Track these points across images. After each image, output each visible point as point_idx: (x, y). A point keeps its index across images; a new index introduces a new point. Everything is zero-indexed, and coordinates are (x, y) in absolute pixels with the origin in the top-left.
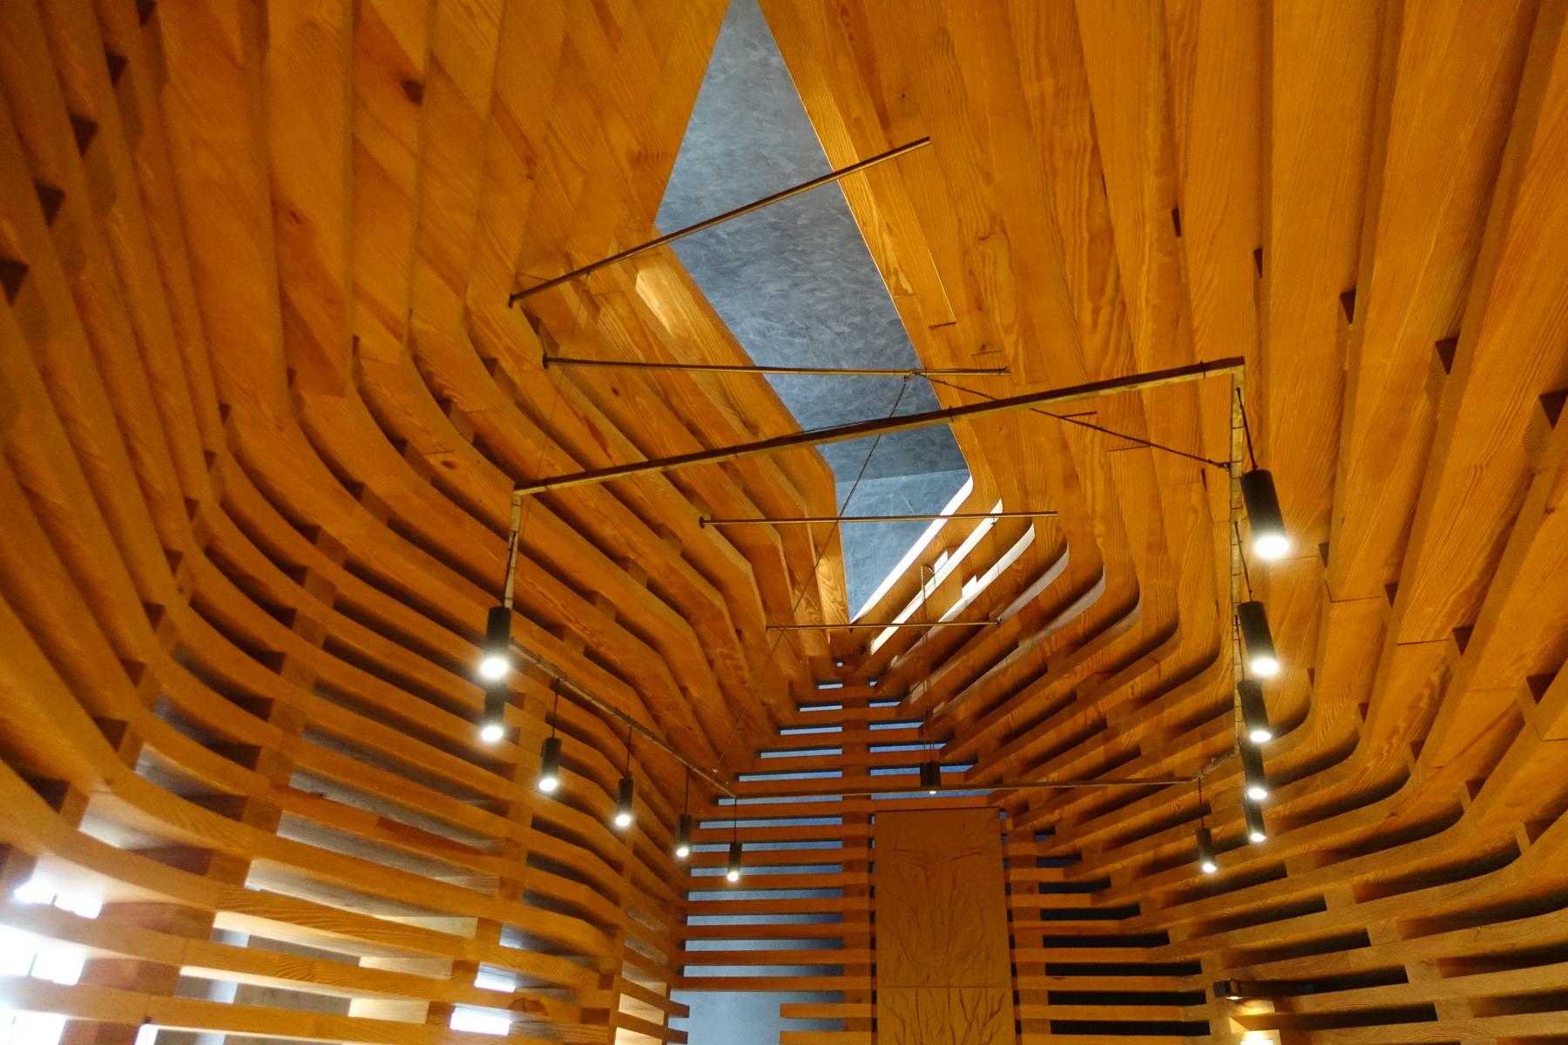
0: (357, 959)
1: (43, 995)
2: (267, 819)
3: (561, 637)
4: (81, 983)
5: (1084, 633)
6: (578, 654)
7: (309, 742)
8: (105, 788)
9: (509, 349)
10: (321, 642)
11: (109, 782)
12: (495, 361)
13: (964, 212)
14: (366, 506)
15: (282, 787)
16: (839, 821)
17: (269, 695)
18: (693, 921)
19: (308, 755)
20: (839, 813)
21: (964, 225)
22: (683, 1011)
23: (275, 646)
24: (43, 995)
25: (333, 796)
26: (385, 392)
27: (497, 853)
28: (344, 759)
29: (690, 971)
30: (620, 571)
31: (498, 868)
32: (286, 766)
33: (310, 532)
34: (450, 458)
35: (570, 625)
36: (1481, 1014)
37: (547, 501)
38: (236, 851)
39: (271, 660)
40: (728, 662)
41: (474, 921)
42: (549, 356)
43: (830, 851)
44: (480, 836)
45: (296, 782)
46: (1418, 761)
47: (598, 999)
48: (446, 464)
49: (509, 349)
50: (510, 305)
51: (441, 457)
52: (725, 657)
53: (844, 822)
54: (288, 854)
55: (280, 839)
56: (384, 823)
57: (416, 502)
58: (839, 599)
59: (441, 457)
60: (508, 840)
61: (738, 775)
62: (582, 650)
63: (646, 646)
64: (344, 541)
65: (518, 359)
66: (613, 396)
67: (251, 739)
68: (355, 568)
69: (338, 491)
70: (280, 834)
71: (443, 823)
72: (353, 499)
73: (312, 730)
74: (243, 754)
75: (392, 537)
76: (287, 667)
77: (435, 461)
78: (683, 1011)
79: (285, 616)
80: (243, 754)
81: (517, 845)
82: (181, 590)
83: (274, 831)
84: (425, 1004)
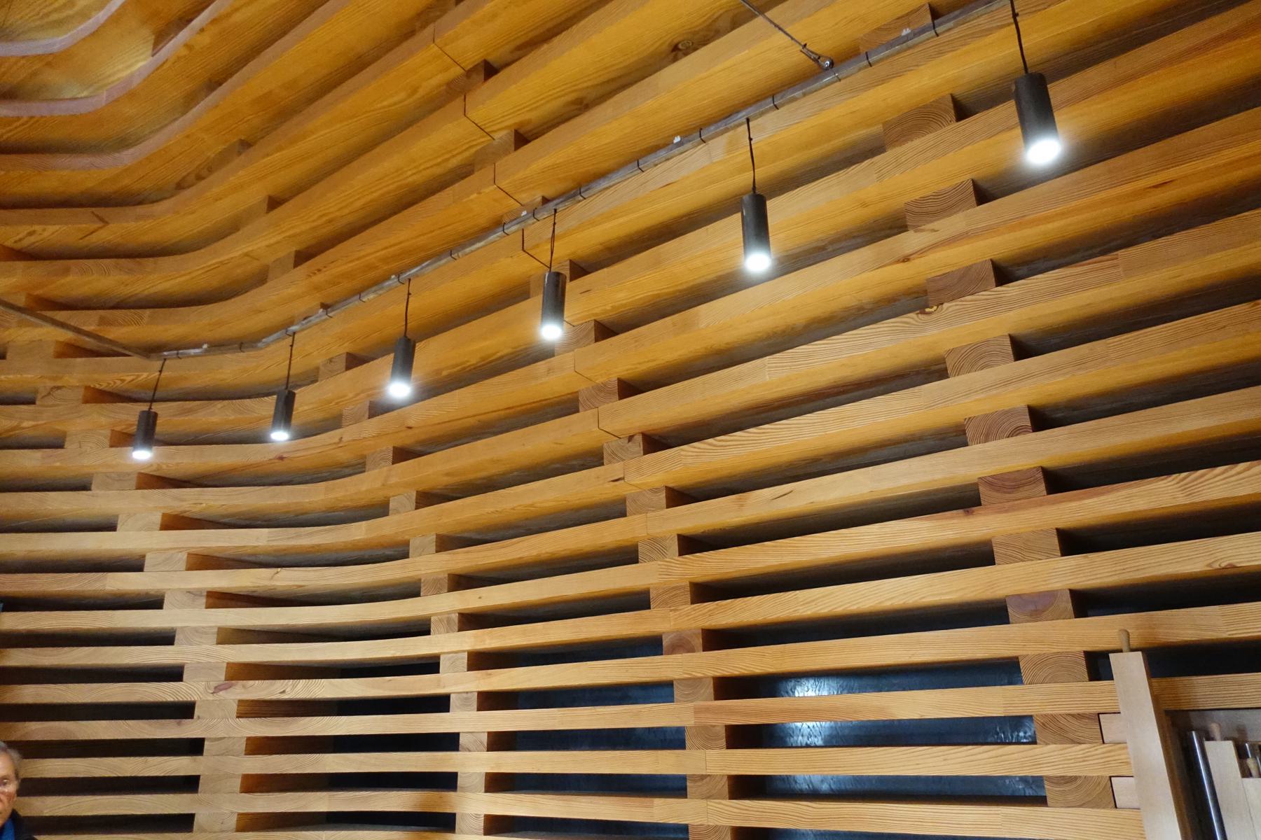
36: (222, 641)
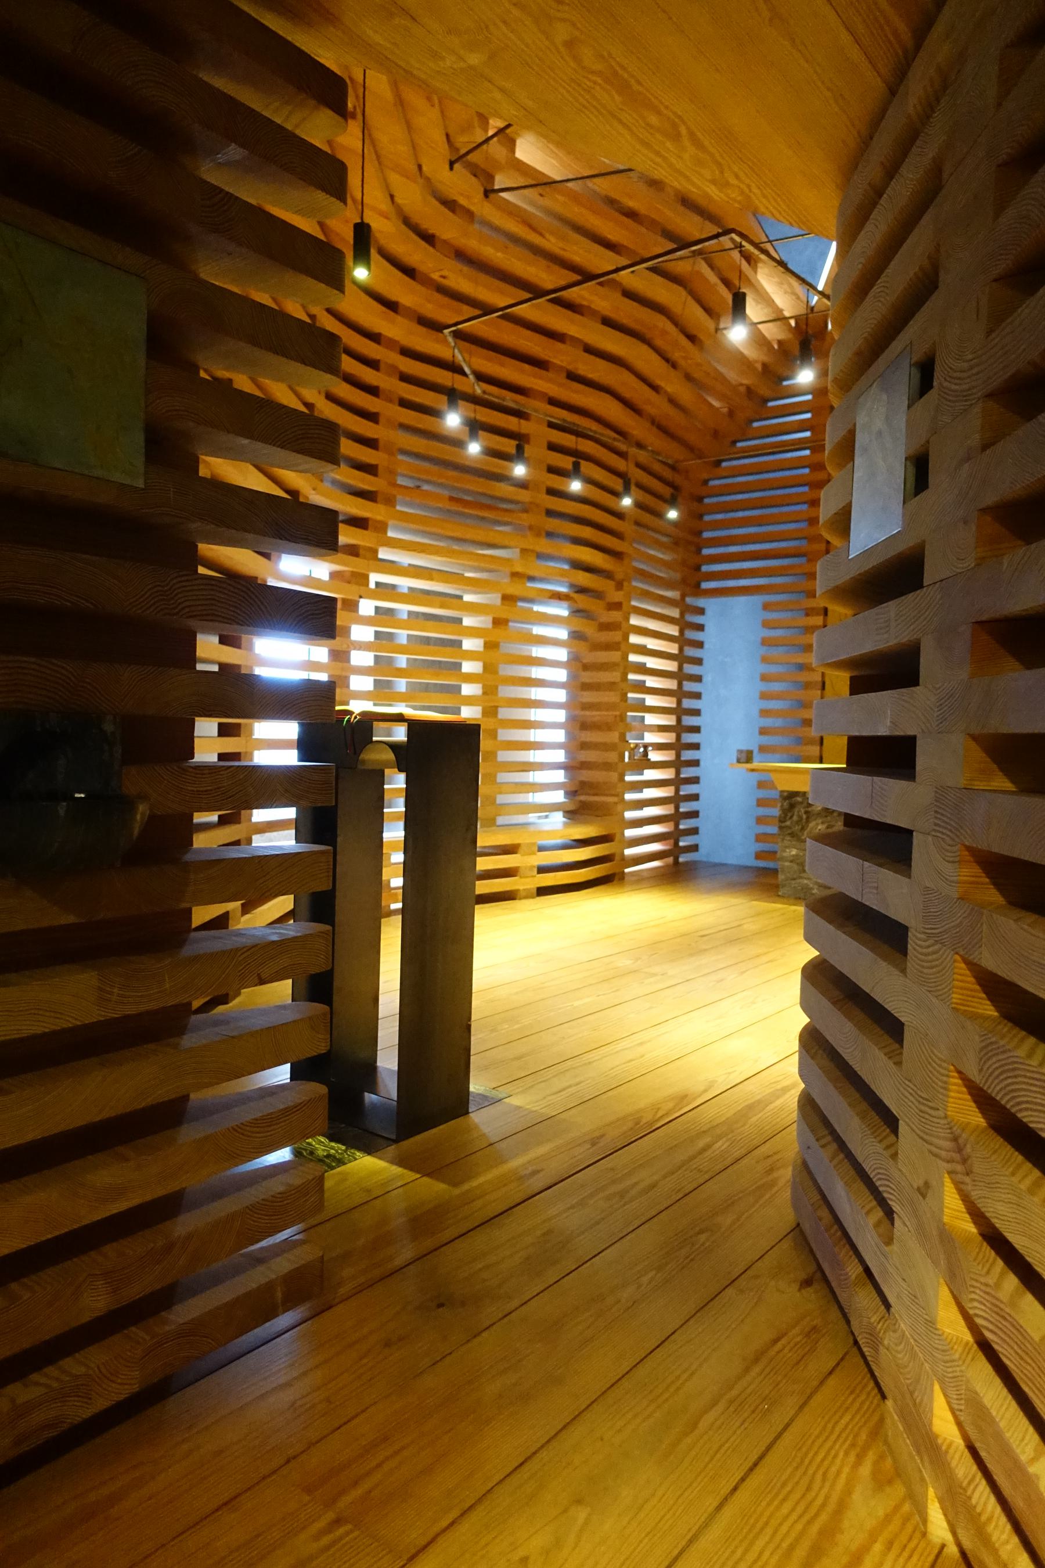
0: (644, 682)
2: (390, 501)
3: (547, 370)
8: (314, 492)
11: (314, 489)
14: (403, 316)
15: (394, 485)
16: (807, 471)
17: (375, 436)
18: (706, 552)
20: (807, 464)
21: (630, 125)
22: (701, 611)
23: (373, 410)
25: (425, 487)
26: (394, 246)
27: (525, 511)
28: (426, 465)
29: (705, 585)
30: (577, 317)
31: (526, 519)
32: (392, 473)
33: (375, 337)
34: (445, 273)
35: (551, 360)
38: (379, 518)
39: (372, 417)
40: (689, 361)
41: (518, 550)
42: (489, 188)
43: (798, 494)
44: (511, 502)
45: (400, 481)
46: (922, 400)
47: (617, 596)
48: (444, 277)
50: (451, 168)
51: (438, 274)
52: (685, 358)
53: (811, 471)
54: (404, 517)
55: (398, 511)
56: (452, 499)
57: (430, 306)
58: (789, 290)
59: (438, 274)
60: (531, 503)
61: (734, 442)
62: (564, 375)
63: (614, 366)
64: (397, 338)
65: (468, 197)
66: (541, 198)
67: (373, 462)
68: (407, 352)
70: (398, 508)
71: (493, 497)
72: (392, 313)
74: (370, 469)
75: (423, 330)
76: (382, 420)
77: (435, 276)
78: (701, 611)
79: (373, 391)
80: (370, 469)
81: (537, 506)
82: (320, 393)
83: (394, 507)
84: (500, 596)
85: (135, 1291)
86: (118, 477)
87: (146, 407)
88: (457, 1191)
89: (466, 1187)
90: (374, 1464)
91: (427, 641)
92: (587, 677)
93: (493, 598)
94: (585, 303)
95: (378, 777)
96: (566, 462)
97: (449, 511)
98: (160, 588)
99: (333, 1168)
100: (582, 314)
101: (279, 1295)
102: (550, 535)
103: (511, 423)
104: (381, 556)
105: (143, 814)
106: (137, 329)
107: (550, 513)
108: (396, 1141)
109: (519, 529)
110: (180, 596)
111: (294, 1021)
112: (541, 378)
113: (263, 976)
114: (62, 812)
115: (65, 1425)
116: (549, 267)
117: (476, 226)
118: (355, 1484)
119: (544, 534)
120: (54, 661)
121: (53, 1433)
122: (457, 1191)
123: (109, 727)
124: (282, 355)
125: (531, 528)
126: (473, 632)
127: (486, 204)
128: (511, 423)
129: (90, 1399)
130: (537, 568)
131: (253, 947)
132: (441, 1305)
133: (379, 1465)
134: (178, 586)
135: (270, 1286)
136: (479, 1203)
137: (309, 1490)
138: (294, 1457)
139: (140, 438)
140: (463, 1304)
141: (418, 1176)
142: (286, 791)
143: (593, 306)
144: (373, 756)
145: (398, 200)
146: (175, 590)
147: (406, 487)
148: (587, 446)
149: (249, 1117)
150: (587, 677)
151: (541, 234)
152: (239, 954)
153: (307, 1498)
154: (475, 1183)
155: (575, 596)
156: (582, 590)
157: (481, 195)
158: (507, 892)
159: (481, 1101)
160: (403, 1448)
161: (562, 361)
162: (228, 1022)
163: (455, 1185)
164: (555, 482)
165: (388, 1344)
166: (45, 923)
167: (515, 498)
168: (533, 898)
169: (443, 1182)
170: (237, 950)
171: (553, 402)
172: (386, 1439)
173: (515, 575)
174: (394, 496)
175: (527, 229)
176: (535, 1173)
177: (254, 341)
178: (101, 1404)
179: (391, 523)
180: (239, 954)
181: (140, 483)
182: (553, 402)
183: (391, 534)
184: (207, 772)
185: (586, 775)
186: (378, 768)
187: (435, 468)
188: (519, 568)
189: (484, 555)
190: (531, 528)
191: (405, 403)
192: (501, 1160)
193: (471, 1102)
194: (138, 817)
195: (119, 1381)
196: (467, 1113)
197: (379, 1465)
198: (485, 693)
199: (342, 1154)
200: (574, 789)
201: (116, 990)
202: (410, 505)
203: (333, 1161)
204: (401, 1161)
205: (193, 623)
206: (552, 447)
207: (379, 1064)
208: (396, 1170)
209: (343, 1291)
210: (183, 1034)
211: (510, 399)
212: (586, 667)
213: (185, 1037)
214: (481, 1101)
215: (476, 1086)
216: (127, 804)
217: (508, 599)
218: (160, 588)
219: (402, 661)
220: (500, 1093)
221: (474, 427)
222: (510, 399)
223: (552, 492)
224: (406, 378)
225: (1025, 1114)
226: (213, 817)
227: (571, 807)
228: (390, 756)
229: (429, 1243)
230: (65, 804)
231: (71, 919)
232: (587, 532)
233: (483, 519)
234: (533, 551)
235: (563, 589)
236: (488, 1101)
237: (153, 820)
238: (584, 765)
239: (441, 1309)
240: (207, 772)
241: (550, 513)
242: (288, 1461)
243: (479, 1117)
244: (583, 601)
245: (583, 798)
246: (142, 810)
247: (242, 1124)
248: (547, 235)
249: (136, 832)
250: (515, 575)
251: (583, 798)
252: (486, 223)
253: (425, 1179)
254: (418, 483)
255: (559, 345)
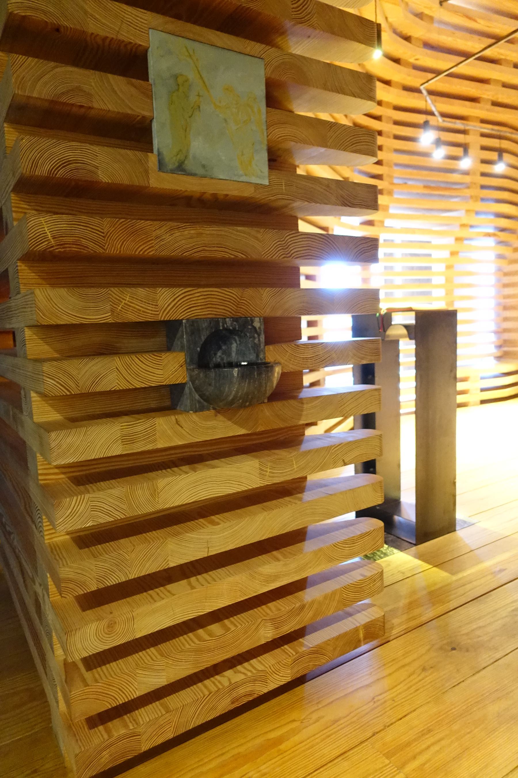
1: (464, 380)
4: (301, 431)
5: (40, 397)
6: (489, 106)
7: (396, 168)
9: (425, 7)
10: (392, 137)
12: (422, 13)
13: (154, 535)
15: (392, 184)
19: (397, 172)
24: (464, 380)
27: (468, 188)
28: (409, 170)
31: (467, 192)
32: (390, 177)
34: (416, 57)
37: (451, 75)
45: (396, 181)
48: (417, 59)
49: (425, 7)
54: (398, 201)
56: (425, 187)
57: (409, 78)
65: (430, 8)
67: (380, 172)
69: (384, 87)
71: (447, 183)
73: (397, 165)
75: (405, 93)
81: (475, 184)
85: (287, 629)
86: (254, 180)
87: (268, 136)
88: (454, 578)
89: (460, 575)
90: (424, 746)
91: (412, 268)
92: (507, 280)
93: (450, 240)
94: (503, 57)
95: (396, 343)
96: (494, 156)
97: (424, 194)
98: (280, 243)
99: (381, 558)
100: (501, 64)
101: (361, 636)
102: (483, 200)
103: (460, 138)
104: (386, 224)
105: (278, 373)
106: (261, 91)
107: (483, 187)
108: (415, 545)
109: (464, 198)
110: (291, 246)
111: (364, 486)
112: (475, 108)
113: (346, 461)
114: (235, 374)
115: (256, 695)
116: (480, 39)
117: (436, 25)
118: (414, 757)
119: (479, 200)
120: (226, 289)
121: (251, 699)
122: (454, 578)
123: (257, 324)
124: (342, 94)
125: (471, 197)
126: (439, 260)
127: (442, 10)
128: (460, 138)
129: (267, 683)
130: (474, 220)
131: (340, 445)
132: (453, 649)
133: (428, 747)
134: (290, 240)
135: (356, 630)
136: (468, 587)
137: (388, 755)
138: (377, 733)
139: (265, 156)
140: (467, 651)
141: (431, 566)
142: (354, 355)
143: (508, 58)
144: (392, 332)
145: (390, 20)
146: (288, 243)
147: (399, 184)
148: (505, 144)
149: (343, 538)
150: (507, 280)
151: (475, 21)
152: (333, 448)
153: (387, 761)
154: (465, 574)
155: (500, 234)
156: (503, 230)
157: (438, 5)
158: (464, 403)
159: (462, 524)
160: (442, 739)
161: (488, 95)
162: (325, 486)
163: (453, 573)
164: (486, 168)
165: (424, 669)
166: (231, 434)
167: (461, 181)
168: (478, 405)
169: (446, 571)
170: (331, 446)
171: (483, 121)
172: (430, 731)
173: (463, 226)
174: (393, 190)
175: (465, 19)
176: (501, 571)
177: (325, 87)
178: (272, 686)
179: (391, 205)
180: (333, 448)
181: (266, 182)
182: (483, 121)
183: (392, 211)
184: (310, 347)
185: (507, 336)
186: (397, 339)
187: (415, 171)
188: (465, 221)
189: (444, 217)
190: (471, 197)
191: (397, 137)
192: (479, 561)
193: (457, 524)
194: (276, 375)
195: (281, 675)
196: (455, 530)
197: (428, 747)
198: (447, 294)
199: (386, 550)
200: (499, 344)
201: (269, 470)
202: (402, 193)
203: (382, 554)
204: (419, 556)
205: (298, 261)
206: (484, 148)
207: (402, 500)
208: (418, 562)
209: (395, 632)
210: (304, 492)
211: (459, 125)
212: (506, 274)
213: (305, 493)
214: (462, 524)
215: (460, 515)
216: (268, 367)
217: (458, 239)
218: (280, 243)
219: (398, 280)
220: (472, 520)
221: (438, 142)
222: (459, 125)
223: (483, 174)
224: (397, 123)
225: (172, 318)
226: (307, 370)
227: (499, 354)
228: (404, 331)
229: (440, 609)
230: (236, 369)
231: (242, 431)
232: (506, 195)
233: (443, 196)
234: (473, 211)
235: (491, 231)
236: (467, 525)
237: (283, 375)
238: (505, 330)
239: (454, 651)
240: (310, 347)
241: (483, 187)
242: (374, 735)
243: (460, 533)
244: (503, 236)
245: (506, 349)
246: (278, 370)
247: (338, 542)
248: (479, 20)
249: (275, 382)
250: (463, 226)
251: (506, 349)
252: (441, 22)
253: (435, 569)
254: (405, 181)
255: (486, 86)
